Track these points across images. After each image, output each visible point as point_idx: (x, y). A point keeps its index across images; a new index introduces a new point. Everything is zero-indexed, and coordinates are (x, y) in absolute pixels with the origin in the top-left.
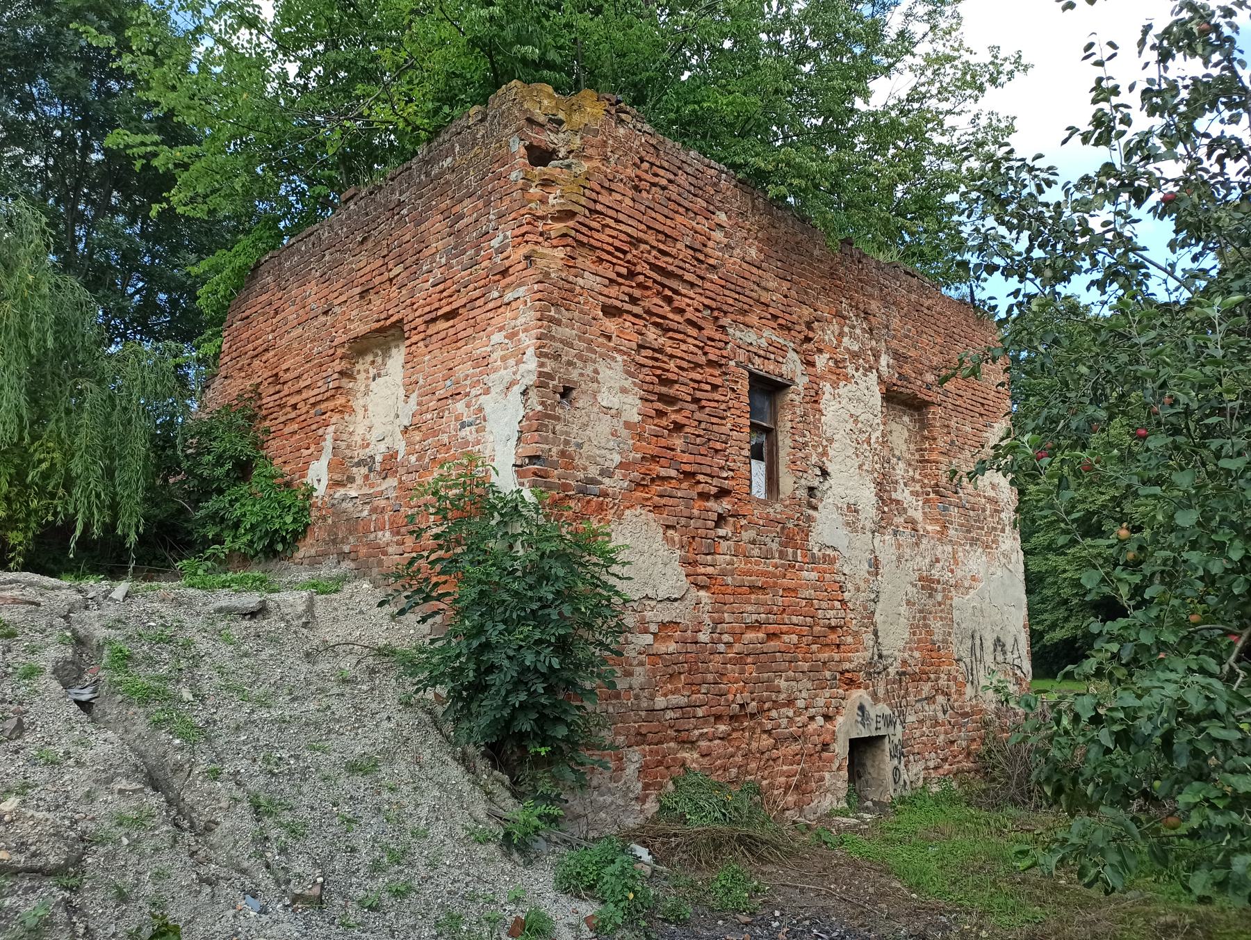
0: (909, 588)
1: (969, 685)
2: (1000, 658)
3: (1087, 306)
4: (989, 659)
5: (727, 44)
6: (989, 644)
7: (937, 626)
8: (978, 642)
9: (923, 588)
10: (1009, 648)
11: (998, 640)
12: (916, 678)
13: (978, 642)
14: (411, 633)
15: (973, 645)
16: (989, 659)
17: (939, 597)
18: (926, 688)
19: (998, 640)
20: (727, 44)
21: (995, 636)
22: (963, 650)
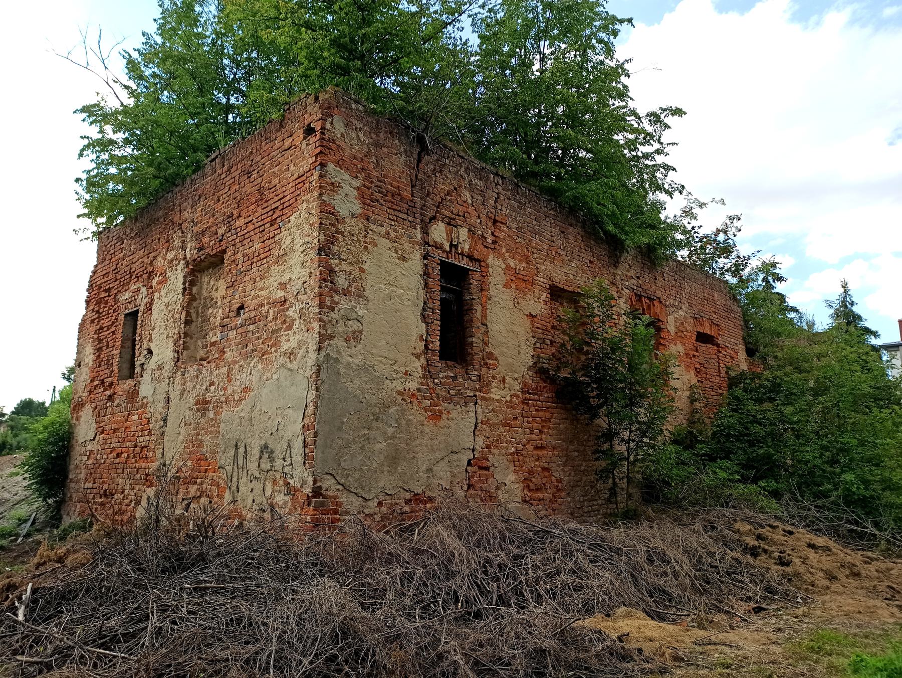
0: (188, 413)
1: (228, 491)
2: (265, 465)
3: (614, 19)
4: (252, 466)
5: (426, 82)
6: (256, 452)
7: (207, 440)
8: (241, 450)
9: (198, 410)
10: (278, 454)
11: (266, 446)
12: (191, 481)
13: (241, 450)
14: (470, 340)
15: (236, 453)
16: (252, 466)
17: (211, 414)
18: (193, 490)
19: (266, 446)
20: (426, 82)
21: (263, 442)
22: (225, 459)
